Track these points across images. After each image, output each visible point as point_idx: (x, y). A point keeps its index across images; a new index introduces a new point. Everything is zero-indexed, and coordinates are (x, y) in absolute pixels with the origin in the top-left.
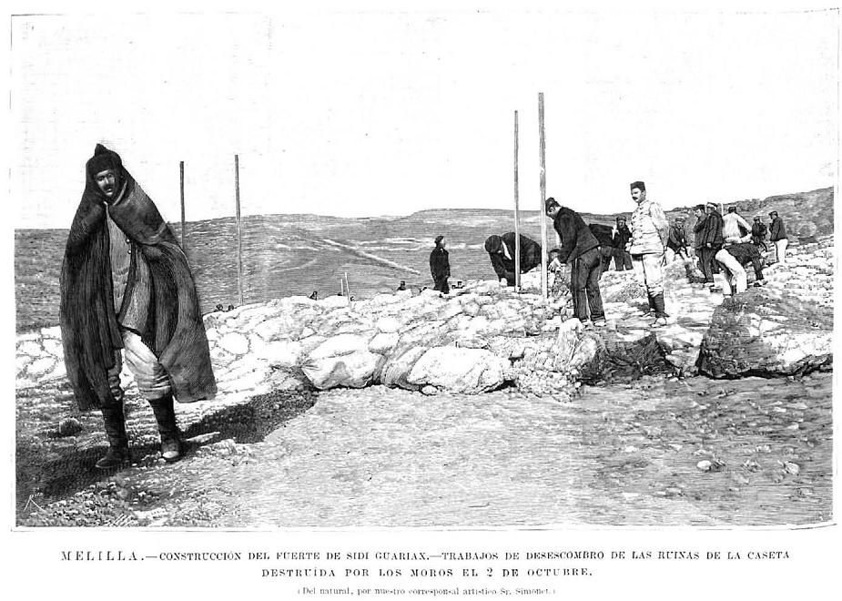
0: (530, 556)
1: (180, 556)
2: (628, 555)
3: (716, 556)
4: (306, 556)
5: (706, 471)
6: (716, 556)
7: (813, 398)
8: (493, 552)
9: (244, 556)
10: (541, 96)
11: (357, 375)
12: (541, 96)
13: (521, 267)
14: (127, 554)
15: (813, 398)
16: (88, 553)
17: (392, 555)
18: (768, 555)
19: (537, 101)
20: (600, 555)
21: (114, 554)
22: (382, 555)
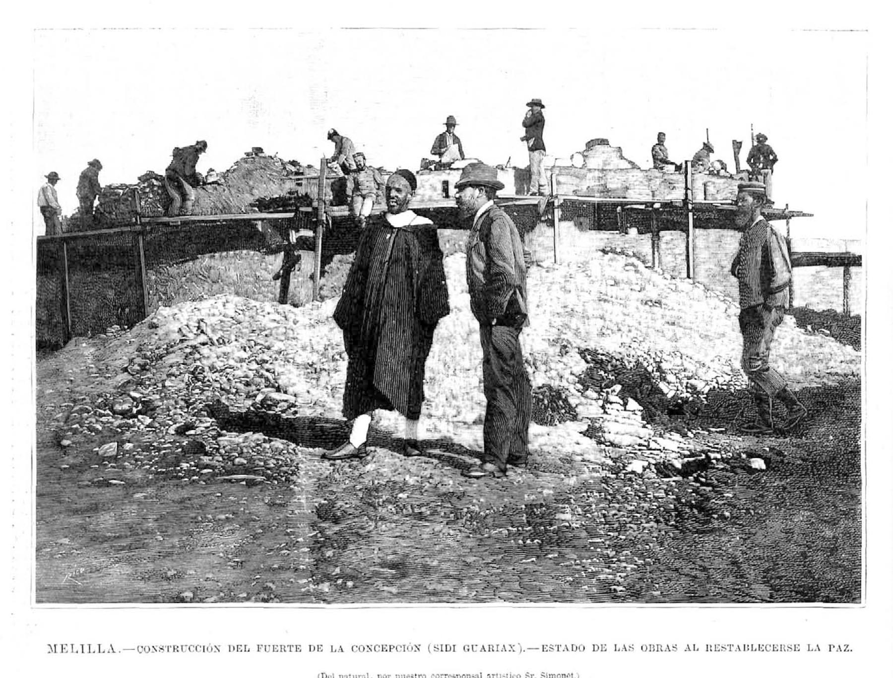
0: (312, 648)
1: (158, 649)
2: (610, 648)
3: (319, 648)
4: (287, 649)
5: (394, 595)
6: (319, 648)
7: (106, 539)
8: (792, 643)
9: (224, 649)
10: (811, 215)
11: (562, 364)
12: (811, 215)
13: (146, 265)
14: (105, 647)
15: (106, 539)
16: (55, 646)
17: (480, 647)
18: (793, 647)
19: (810, 213)
20: (644, 648)
21: (95, 648)
22: (470, 648)
